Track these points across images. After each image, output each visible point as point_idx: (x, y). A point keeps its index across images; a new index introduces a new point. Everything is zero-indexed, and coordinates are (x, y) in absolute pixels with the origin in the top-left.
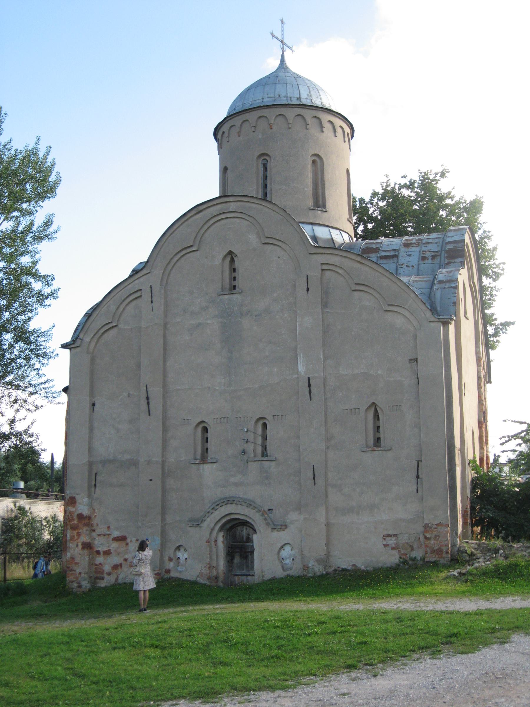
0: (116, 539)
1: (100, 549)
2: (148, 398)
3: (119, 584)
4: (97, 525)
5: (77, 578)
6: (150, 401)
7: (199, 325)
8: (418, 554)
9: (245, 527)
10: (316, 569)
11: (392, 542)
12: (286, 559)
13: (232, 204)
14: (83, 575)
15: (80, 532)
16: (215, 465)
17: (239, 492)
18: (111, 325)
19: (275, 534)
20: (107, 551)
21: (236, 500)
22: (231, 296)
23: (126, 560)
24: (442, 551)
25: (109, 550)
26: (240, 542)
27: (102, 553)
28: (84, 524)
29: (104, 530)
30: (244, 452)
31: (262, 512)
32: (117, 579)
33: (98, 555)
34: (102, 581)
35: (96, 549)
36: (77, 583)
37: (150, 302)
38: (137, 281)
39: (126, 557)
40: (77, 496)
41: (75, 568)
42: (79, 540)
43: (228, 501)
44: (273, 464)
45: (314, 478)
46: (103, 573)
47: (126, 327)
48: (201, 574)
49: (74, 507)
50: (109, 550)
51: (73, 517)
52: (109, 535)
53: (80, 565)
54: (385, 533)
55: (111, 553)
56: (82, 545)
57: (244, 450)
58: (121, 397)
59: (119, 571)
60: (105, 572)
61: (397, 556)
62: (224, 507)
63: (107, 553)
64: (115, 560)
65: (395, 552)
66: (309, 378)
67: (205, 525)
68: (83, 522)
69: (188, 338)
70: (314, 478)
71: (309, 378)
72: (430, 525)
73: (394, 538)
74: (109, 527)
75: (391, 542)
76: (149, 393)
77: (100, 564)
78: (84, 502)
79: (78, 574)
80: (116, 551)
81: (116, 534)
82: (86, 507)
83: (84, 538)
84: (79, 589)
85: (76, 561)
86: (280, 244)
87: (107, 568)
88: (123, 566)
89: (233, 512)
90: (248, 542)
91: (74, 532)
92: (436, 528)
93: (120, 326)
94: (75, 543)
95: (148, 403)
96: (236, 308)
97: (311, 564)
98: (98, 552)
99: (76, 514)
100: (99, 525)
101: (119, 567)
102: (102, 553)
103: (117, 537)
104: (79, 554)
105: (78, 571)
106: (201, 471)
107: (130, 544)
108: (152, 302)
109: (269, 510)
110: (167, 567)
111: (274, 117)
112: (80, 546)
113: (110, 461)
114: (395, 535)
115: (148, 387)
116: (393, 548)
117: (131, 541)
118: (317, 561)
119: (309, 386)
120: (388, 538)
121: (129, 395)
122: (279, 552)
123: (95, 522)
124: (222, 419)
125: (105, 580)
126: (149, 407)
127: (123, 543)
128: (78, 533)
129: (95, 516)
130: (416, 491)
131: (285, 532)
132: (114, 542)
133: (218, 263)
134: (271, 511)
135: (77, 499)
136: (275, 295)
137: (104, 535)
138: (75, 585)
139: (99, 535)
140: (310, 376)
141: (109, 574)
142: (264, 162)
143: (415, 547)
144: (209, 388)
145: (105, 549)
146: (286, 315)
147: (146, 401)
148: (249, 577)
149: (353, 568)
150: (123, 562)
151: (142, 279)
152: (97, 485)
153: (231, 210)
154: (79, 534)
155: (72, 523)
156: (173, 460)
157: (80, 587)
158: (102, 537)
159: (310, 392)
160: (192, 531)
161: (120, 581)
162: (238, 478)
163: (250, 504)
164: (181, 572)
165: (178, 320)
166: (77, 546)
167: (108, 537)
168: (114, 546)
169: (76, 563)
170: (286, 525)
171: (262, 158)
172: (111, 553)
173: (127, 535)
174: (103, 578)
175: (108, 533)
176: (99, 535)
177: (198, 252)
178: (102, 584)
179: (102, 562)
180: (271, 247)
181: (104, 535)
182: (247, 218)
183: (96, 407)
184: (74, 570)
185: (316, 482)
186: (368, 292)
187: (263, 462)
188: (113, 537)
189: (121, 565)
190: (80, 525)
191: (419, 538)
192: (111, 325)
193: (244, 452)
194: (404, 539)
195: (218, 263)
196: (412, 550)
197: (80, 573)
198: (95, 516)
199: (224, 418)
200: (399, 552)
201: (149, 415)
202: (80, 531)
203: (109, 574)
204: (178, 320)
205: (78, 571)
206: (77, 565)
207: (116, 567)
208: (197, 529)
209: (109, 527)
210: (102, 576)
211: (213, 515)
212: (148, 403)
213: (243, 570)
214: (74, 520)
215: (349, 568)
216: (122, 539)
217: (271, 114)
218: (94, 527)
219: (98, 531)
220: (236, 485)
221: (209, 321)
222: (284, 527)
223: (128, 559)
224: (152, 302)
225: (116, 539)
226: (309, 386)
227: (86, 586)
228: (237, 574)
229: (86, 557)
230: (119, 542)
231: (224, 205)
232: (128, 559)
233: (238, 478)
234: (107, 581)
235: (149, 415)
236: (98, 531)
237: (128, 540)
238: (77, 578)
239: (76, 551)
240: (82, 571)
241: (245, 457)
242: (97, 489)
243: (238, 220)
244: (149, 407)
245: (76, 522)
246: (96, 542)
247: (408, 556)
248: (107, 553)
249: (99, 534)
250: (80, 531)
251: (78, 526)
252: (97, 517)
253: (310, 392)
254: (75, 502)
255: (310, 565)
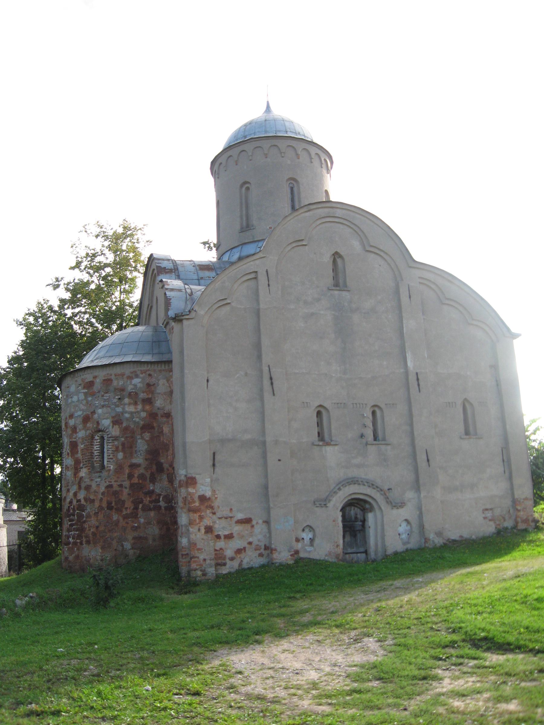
0: (240, 522)
1: (220, 533)
2: (271, 379)
3: (244, 570)
4: (219, 507)
5: (201, 565)
6: (273, 381)
7: (312, 314)
8: (509, 524)
9: (353, 508)
10: (436, 541)
11: (489, 514)
12: (402, 534)
13: (338, 210)
14: (208, 562)
15: (203, 515)
16: (336, 447)
17: (360, 473)
18: (225, 302)
19: (395, 511)
20: (228, 534)
21: (360, 480)
22: (341, 292)
23: (250, 543)
24: (528, 520)
25: (232, 534)
26: (349, 522)
27: (222, 537)
28: (207, 506)
29: (227, 513)
30: (362, 436)
31: (380, 490)
32: (240, 565)
33: (218, 540)
34: (223, 567)
35: (216, 534)
36: (201, 571)
37: (267, 285)
38: (252, 263)
39: (251, 540)
40: (197, 477)
41: (197, 555)
42: (202, 523)
43: (353, 481)
44: (389, 447)
45: (428, 460)
46: (224, 558)
47: (239, 306)
48: (330, 553)
49: (194, 488)
50: (232, 534)
51: (193, 499)
52: (231, 517)
53: (203, 550)
54: (484, 507)
55: (233, 537)
56: (205, 529)
57: (362, 434)
58: (237, 375)
59: (243, 555)
60: (227, 557)
61: (494, 526)
62: (347, 487)
63: (229, 537)
64: (237, 544)
65: (492, 523)
66: (417, 374)
67: (330, 505)
68: (206, 504)
69: (303, 325)
70: (428, 460)
71: (417, 374)
72: (519, 499)
73: (490, 512)
74: (231, 510)
75: (489, 515)
76: (272, 373)
77: (221, 549)
78: (206, 482)
79: (202, 561)
80: (239, 534)
81: (240, 516)
82: (208, 488)
83: (207, 522)
84: (203, 578)
85: (198, 547)
86: (382, 254)
87: (229, 553)
88: (247, 549)
89: (356, 491)
90: (356, 522)
91: (195, 515)
92: (523, 502)
93: (233, 304)
94: (197, 527)
95: (272, 384)
96: (346, 304)
97: (432, 536)
98: (218, 537)
99: (196, 496)
100: (221, 507)
101: (243, 551)
102: (222, 537)
103: (241, 519)
104: (202, 539)
105: (202, 557)
106: (324, 452)
107: (255, 526)
108: (269, 285)
109: (389, 489)
110: (295, 548)
111: (301, 150)
112: (203, 530)
113: (229, 440)
114: (491, 509)
115: (271, 367)
116: (490, 520)
117: (257, 523)
118: (436, 533)
119: (418, 379)
120: (487, 512)
121: (246, 374)
122: (314, 536)
123: (216, 504)
124: (339, 405)
125: (228, 566)
126: (273, 388)
127: (248, 526)
128: (200, 516)
129: (216, 498)
130: (503, 472)
131: (403, 509)
132: (237, 524)
133: (326, 261)
134: (390, 490)
135: (197, 479)
136: (379, 297)
137: (226, 518)
138: (199, 573)
139: (220, 518)
140: (418, 371)
141: (232, 559)
142: (291, 186)
143: (507, 517)
144: (326, 374)
145: (227, 533)
146: (390, 316)
147: (270, 382)
148: (359, 555)
149: (460, 539)
150: (247, 546)
151: (257, 262)
152: (217, 464)
153: (337, 215)
154: (201, 518)
155: (193, 505)
156: (295, 441)
157: (204, 575)
158: (223, 520)
159: (419, 385)
160: (318, 510)
161: (245, 566)
162: (358, 460)
163: (372, 485)
164: (310, 552)
165: (292, 306)
166: (199, 530)
167: (231, 520)
168: (237, 529)
169: (199, 549)
170: (404, 503)
171: (292, 182)
172: (233, 537)
173: (252, 517)
174: (225, 564)
175: (230, 515)
176: (220, 518)
177: (307, 247)
178: (224, 571)
179: (223, 547)
180: (373, 255)
181: (226, 518)
182: (352, 226)
183: (210, 383)
184: (196, 557)
185: (430, 464)
186: (454, 307)
187: (381, 446)
188: (236, 520)
189: (245, 548)
190: (203, 508)
191: (509, 510)
192: (225, 302)
193: (362, 436)
194: (498, 512)
195: (326, 261)
196: (505, 520)
197: (205, 560)
198: (216, 498)
199: (341, 403)
200: (495, 523)
201: (274, 395)
202: (203, 514)
203: (232, 559)
204: (292, 306)
205: (202, 557)
206: (200, 551)
207: (239, 551)
208: (324, 509)
209: (231, 510)
210: (224, 561)
211: (338, 495)
212: (272, 384)
213: (353, 548)
214: (194, 502)
215: (457, 539)
216: (248, 521)
217: (266, 144)
218: (215, 510)
219: (219, 514)
220: (359, 466)
221: (322, 312)
222: (401, 505)
223: (252, 542)
224: (269, 285)
225: (240, 522)
226: (418, 379)
227: (212, 574)
228: (349, 552)
229: (210, 542)
230: (243, 525)
231: (330, 209)
232: (252, 542)
233: (358, 460)
234: (231, 567)
235: (274, 395)
236: (219, 514)
237: (254, 522)
238: (201, 565)
239: (198, 536)
240: (206, 557)
241: (364, 441)
242: (217, 469)
243: (341, 226)
244: (273, 388)
245: (197, 504)
246: (216, 526)
247: (501, 526)
248: (229, 537)
249: (220, 517)
250: (203, 514)
251: (200, 509)
252: (218, 498)
253: (419, 385)
254: (196, 483)
255: (431, 538)
